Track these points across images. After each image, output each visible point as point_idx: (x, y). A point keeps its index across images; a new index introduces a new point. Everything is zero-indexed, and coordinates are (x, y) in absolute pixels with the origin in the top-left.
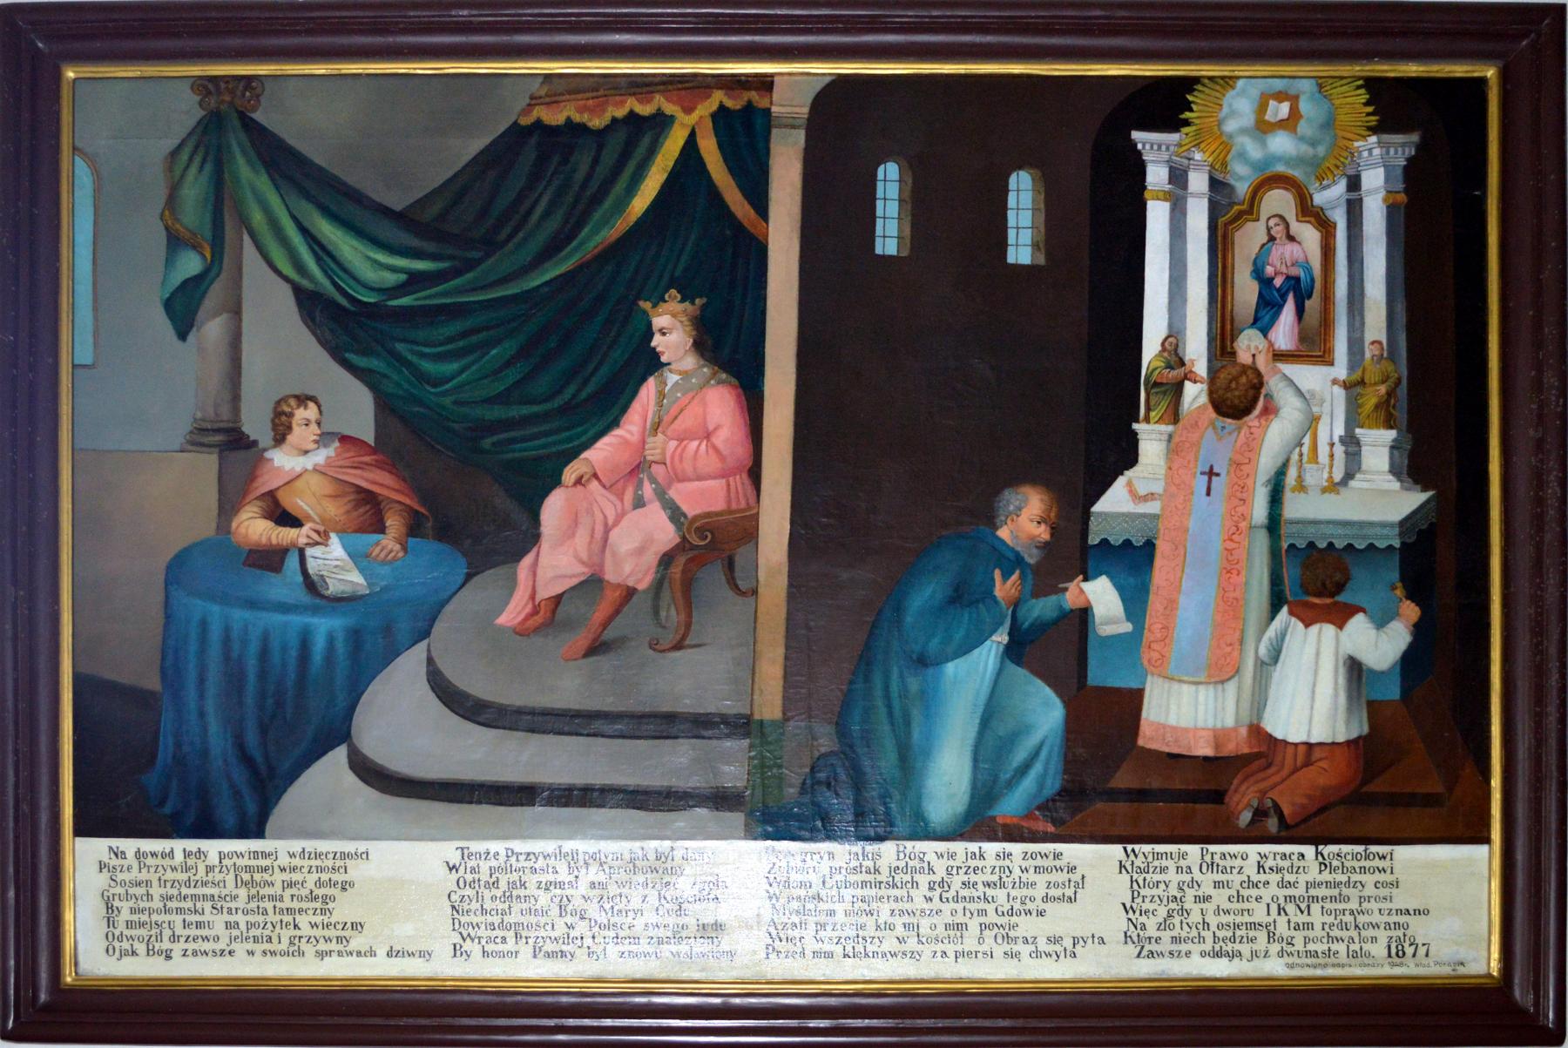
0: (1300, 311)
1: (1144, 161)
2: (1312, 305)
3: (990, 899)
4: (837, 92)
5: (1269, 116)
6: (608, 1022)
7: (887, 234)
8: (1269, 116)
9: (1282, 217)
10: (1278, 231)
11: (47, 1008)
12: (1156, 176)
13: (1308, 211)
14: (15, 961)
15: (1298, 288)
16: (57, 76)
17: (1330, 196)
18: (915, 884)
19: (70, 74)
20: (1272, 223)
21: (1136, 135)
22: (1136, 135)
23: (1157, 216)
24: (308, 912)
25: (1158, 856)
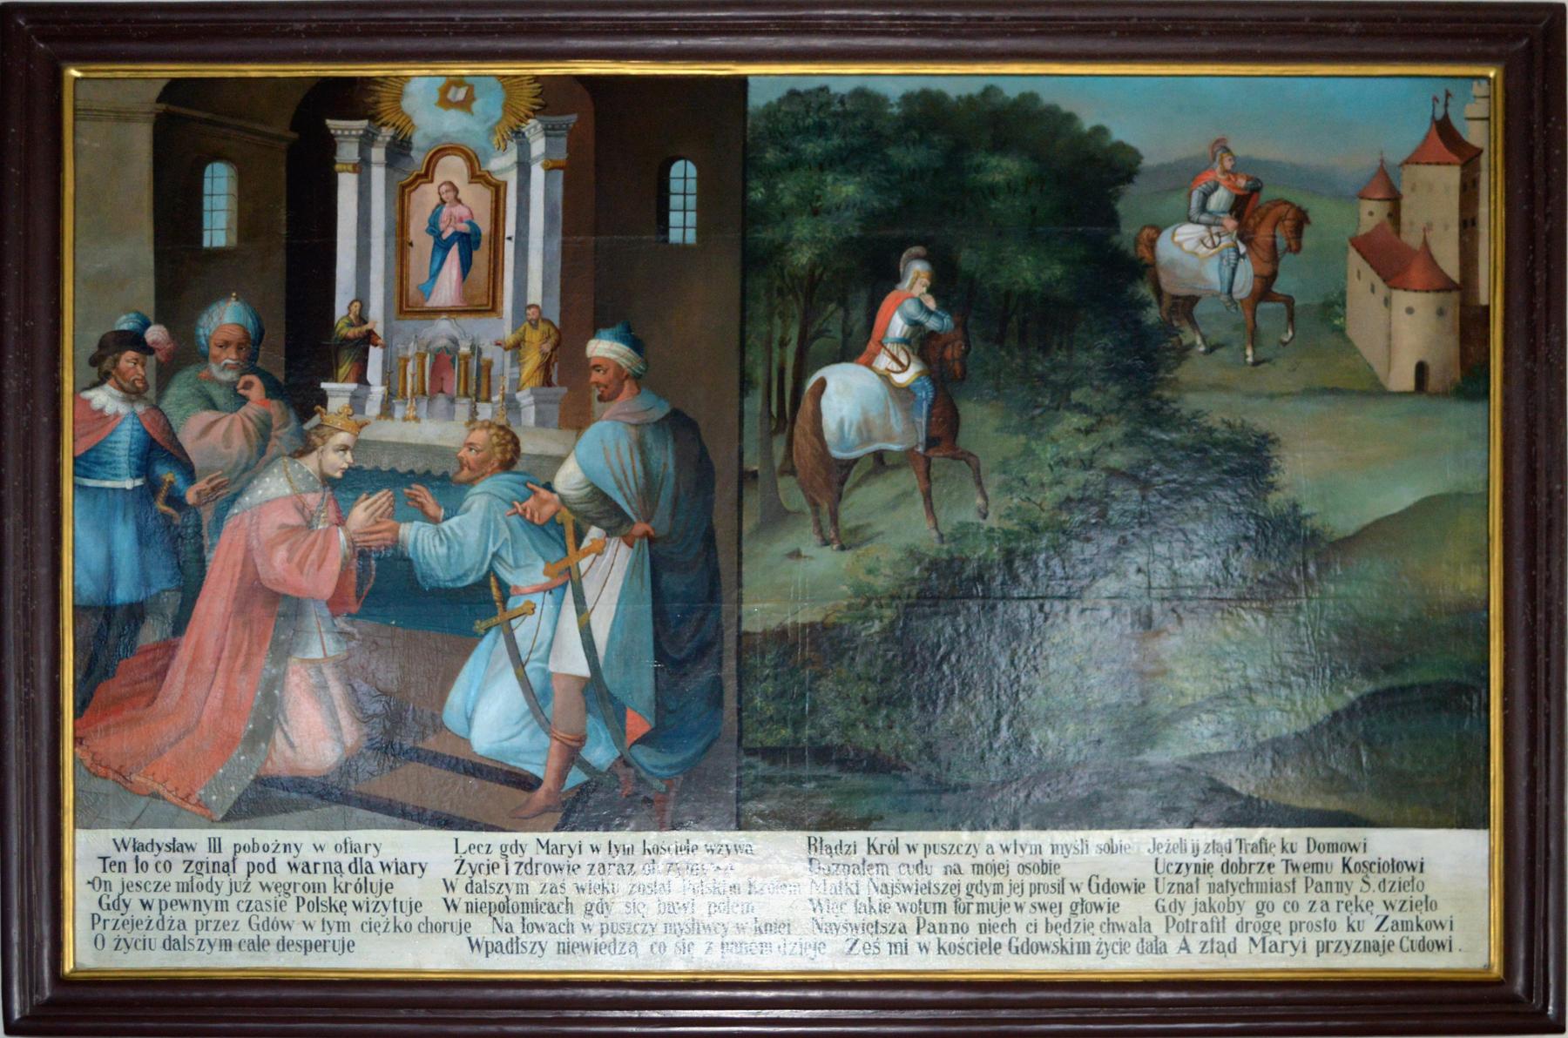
0: (466, 265)
1: (333, 136)
2: (481, 257)
3: (1355, 926)
4: (174, 89)
5: (450, 96)
6: (618, 1014)
7: (682, 191)
8: (450, 96)
9: (451, 183)
10: (449, 196)
11: (51, 1003)
12: (348, 152)
13: (478, 175)
14: (221, 999)
15: (468, 241)
16: (57, 79)
17: (502, 164)
18: (1231, 907)
19: (74, 73)
20: (444, 188)
21: (329, 122)
22: (329, 122)
23: (347, 187)
24: (149, 887)
25: (1313, 845)
